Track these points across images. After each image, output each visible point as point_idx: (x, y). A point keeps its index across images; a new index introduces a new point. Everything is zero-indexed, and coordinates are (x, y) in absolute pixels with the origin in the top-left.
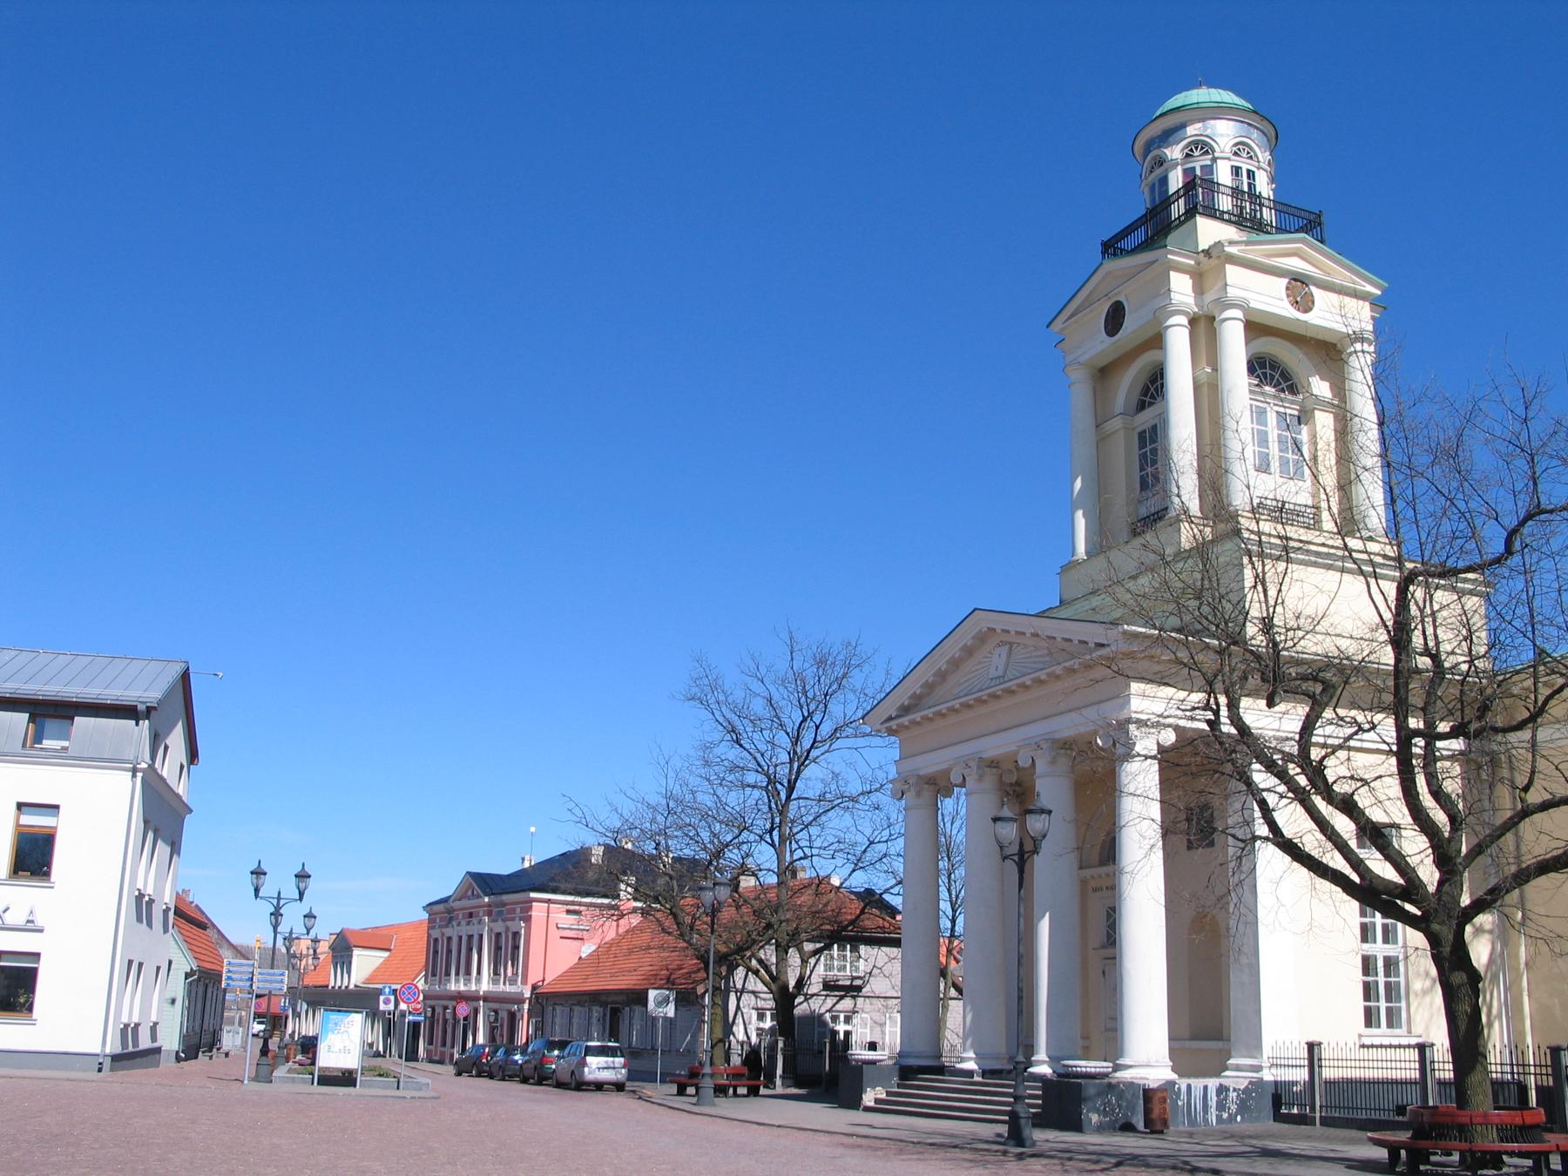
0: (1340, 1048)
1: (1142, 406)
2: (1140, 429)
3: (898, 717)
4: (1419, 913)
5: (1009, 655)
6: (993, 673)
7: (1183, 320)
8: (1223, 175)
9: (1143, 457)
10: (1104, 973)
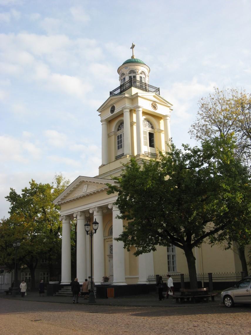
0: (239, 273)
1: (118, 130)
2: (118, 135)
3: (61, 201)
4: (182, 245)
5: (88, 186)
7: (128, 110)
8: (138, 78)
9: (118, 142)
10: (109, 261)
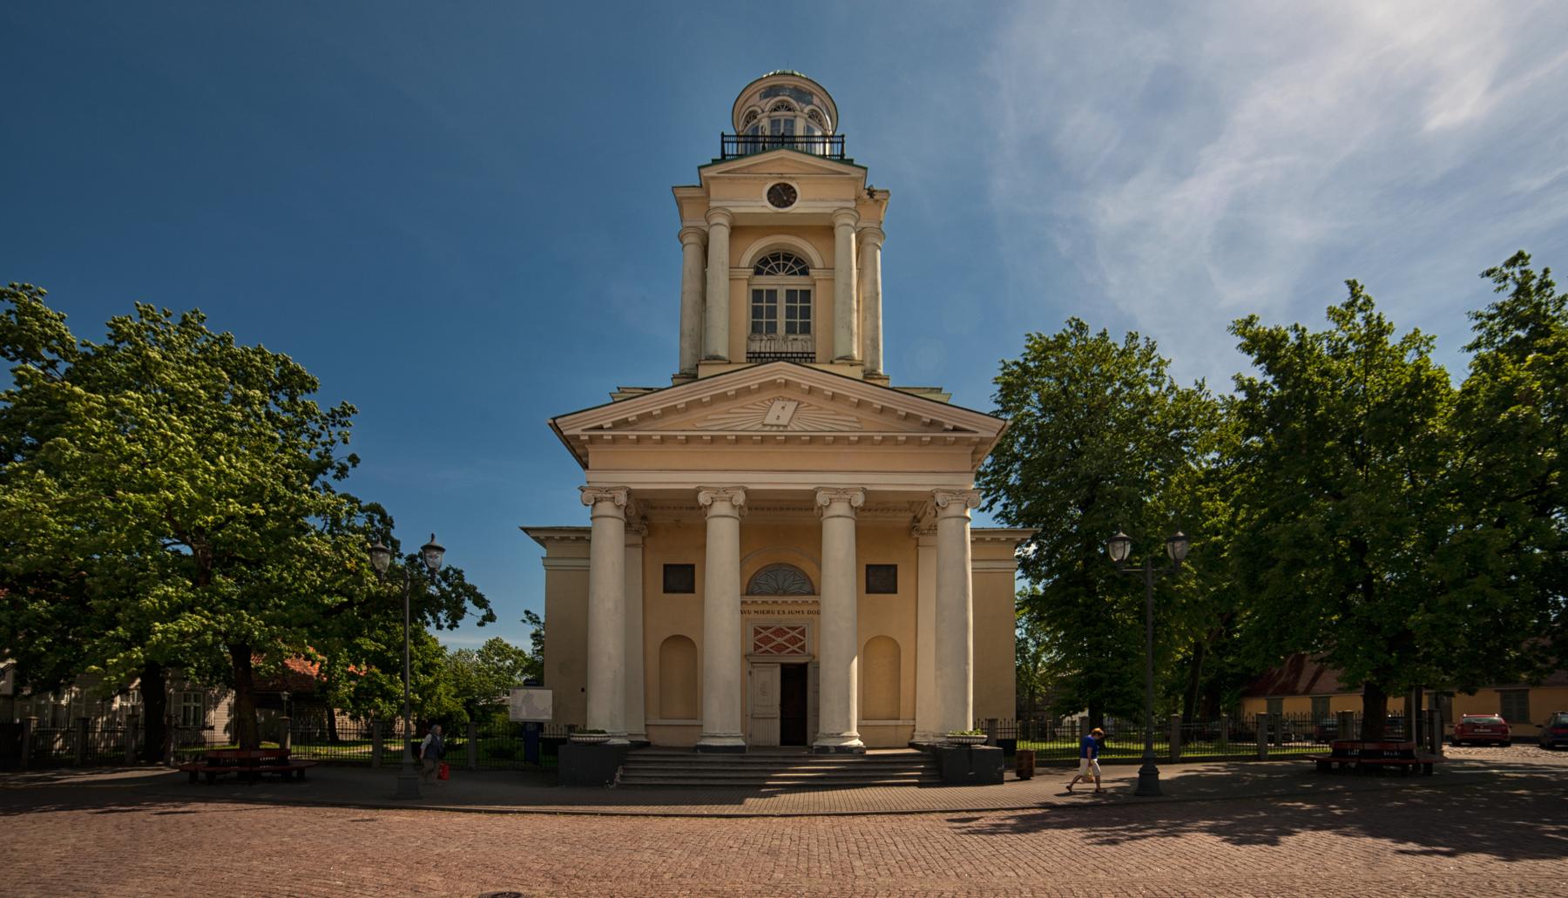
3: (609, 429)
6: (770, 419)
